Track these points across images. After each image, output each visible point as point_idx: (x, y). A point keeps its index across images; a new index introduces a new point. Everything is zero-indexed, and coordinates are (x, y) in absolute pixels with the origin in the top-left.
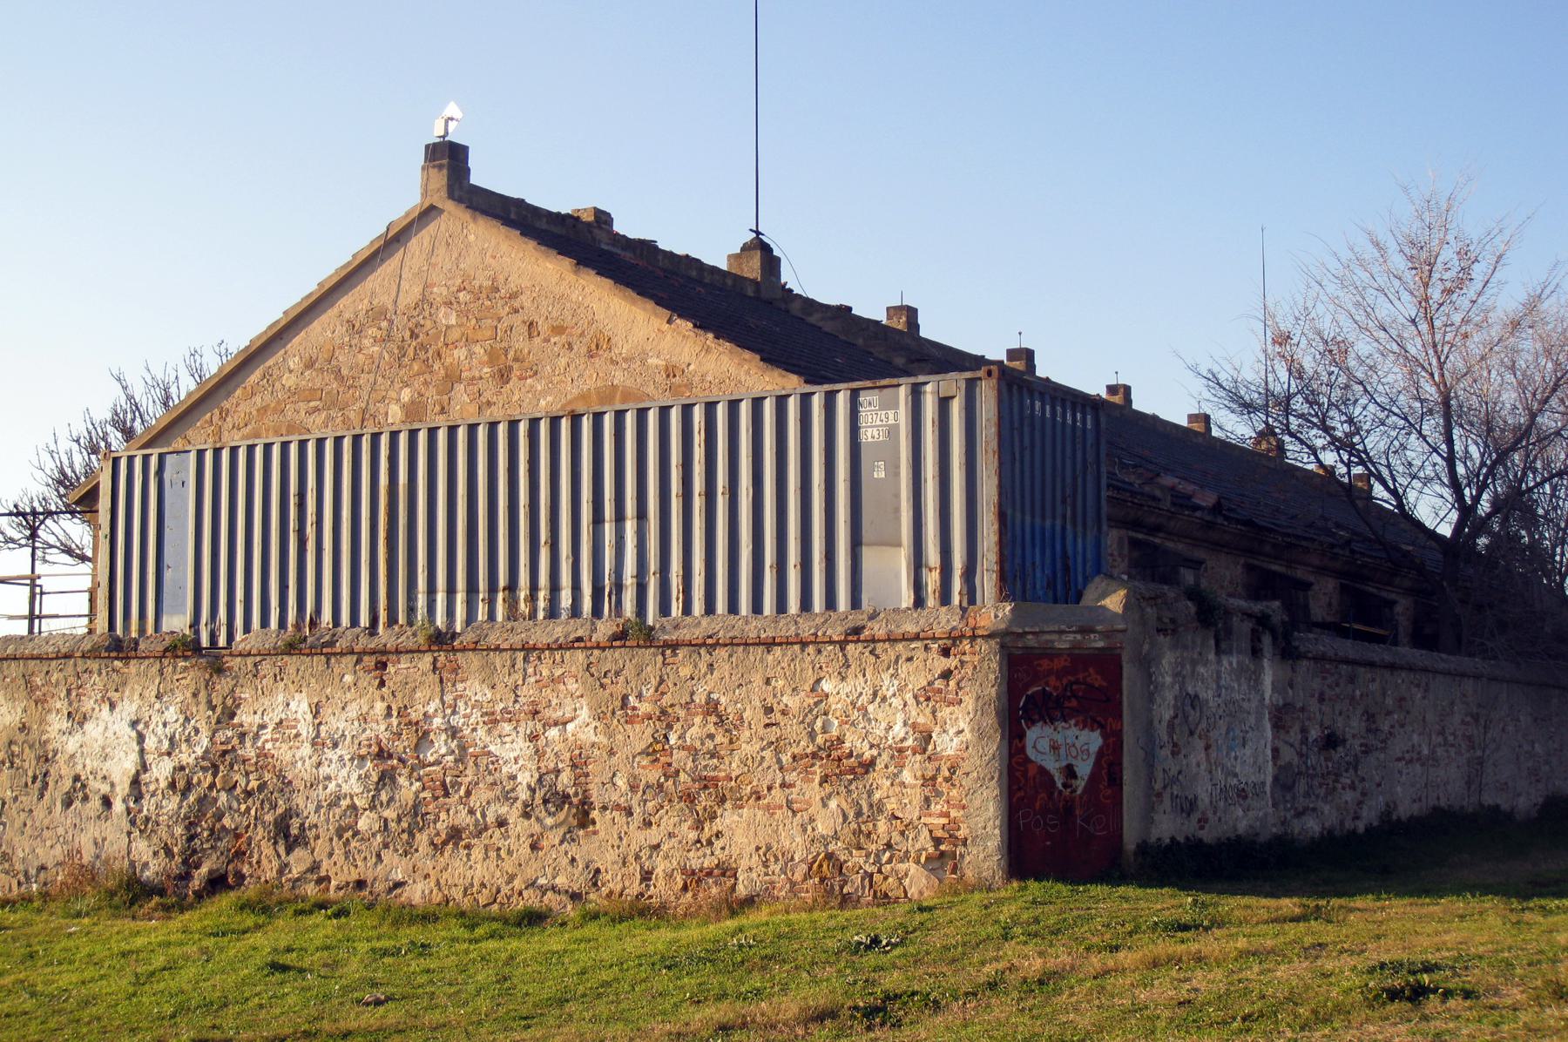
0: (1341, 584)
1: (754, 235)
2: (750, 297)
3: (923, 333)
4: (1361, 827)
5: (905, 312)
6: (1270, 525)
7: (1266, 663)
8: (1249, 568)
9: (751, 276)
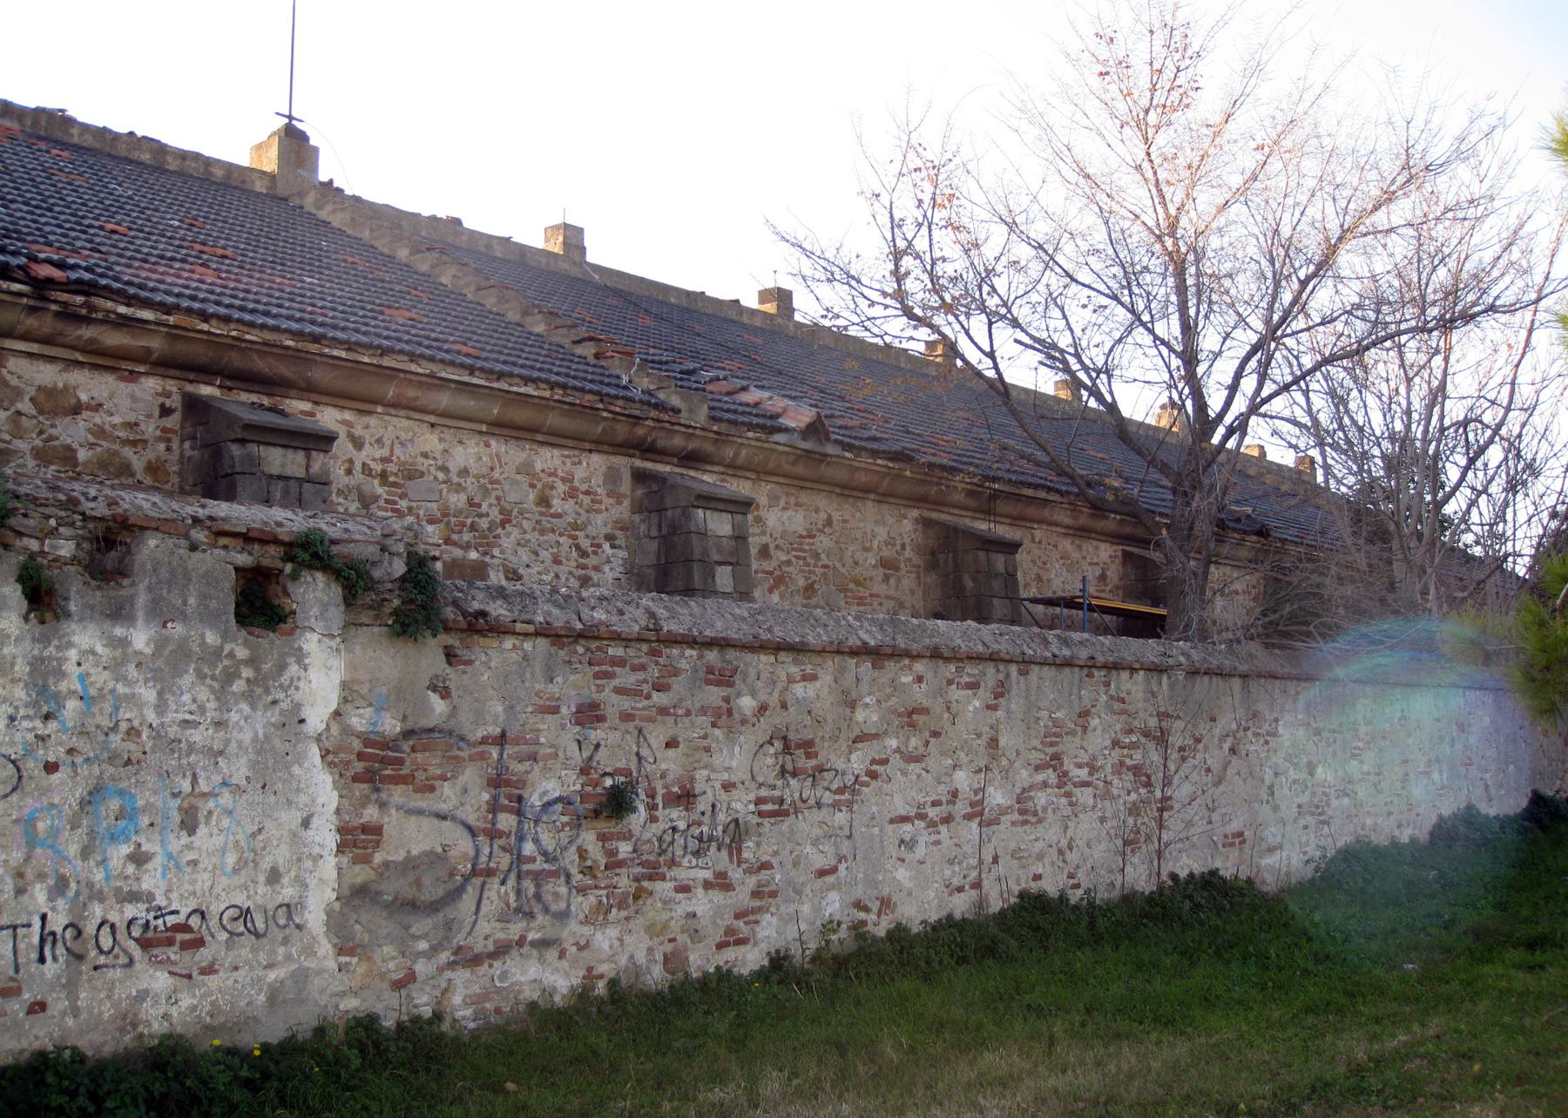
0: (1125, 553)
1: (287, 121)
2: (258, 195)
3: (591, 258)
4: (750, 959)
5: (562, 231)
6: (955, 464)
7: (311, 643)
8: (927, 523)
9: (267, 169)
